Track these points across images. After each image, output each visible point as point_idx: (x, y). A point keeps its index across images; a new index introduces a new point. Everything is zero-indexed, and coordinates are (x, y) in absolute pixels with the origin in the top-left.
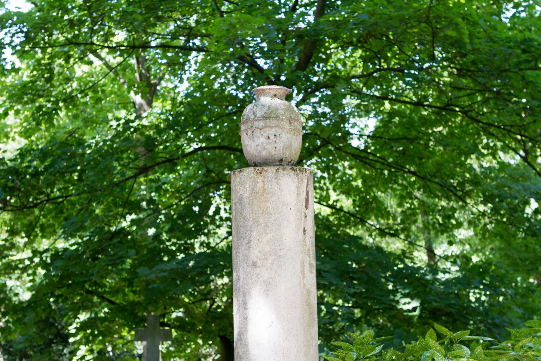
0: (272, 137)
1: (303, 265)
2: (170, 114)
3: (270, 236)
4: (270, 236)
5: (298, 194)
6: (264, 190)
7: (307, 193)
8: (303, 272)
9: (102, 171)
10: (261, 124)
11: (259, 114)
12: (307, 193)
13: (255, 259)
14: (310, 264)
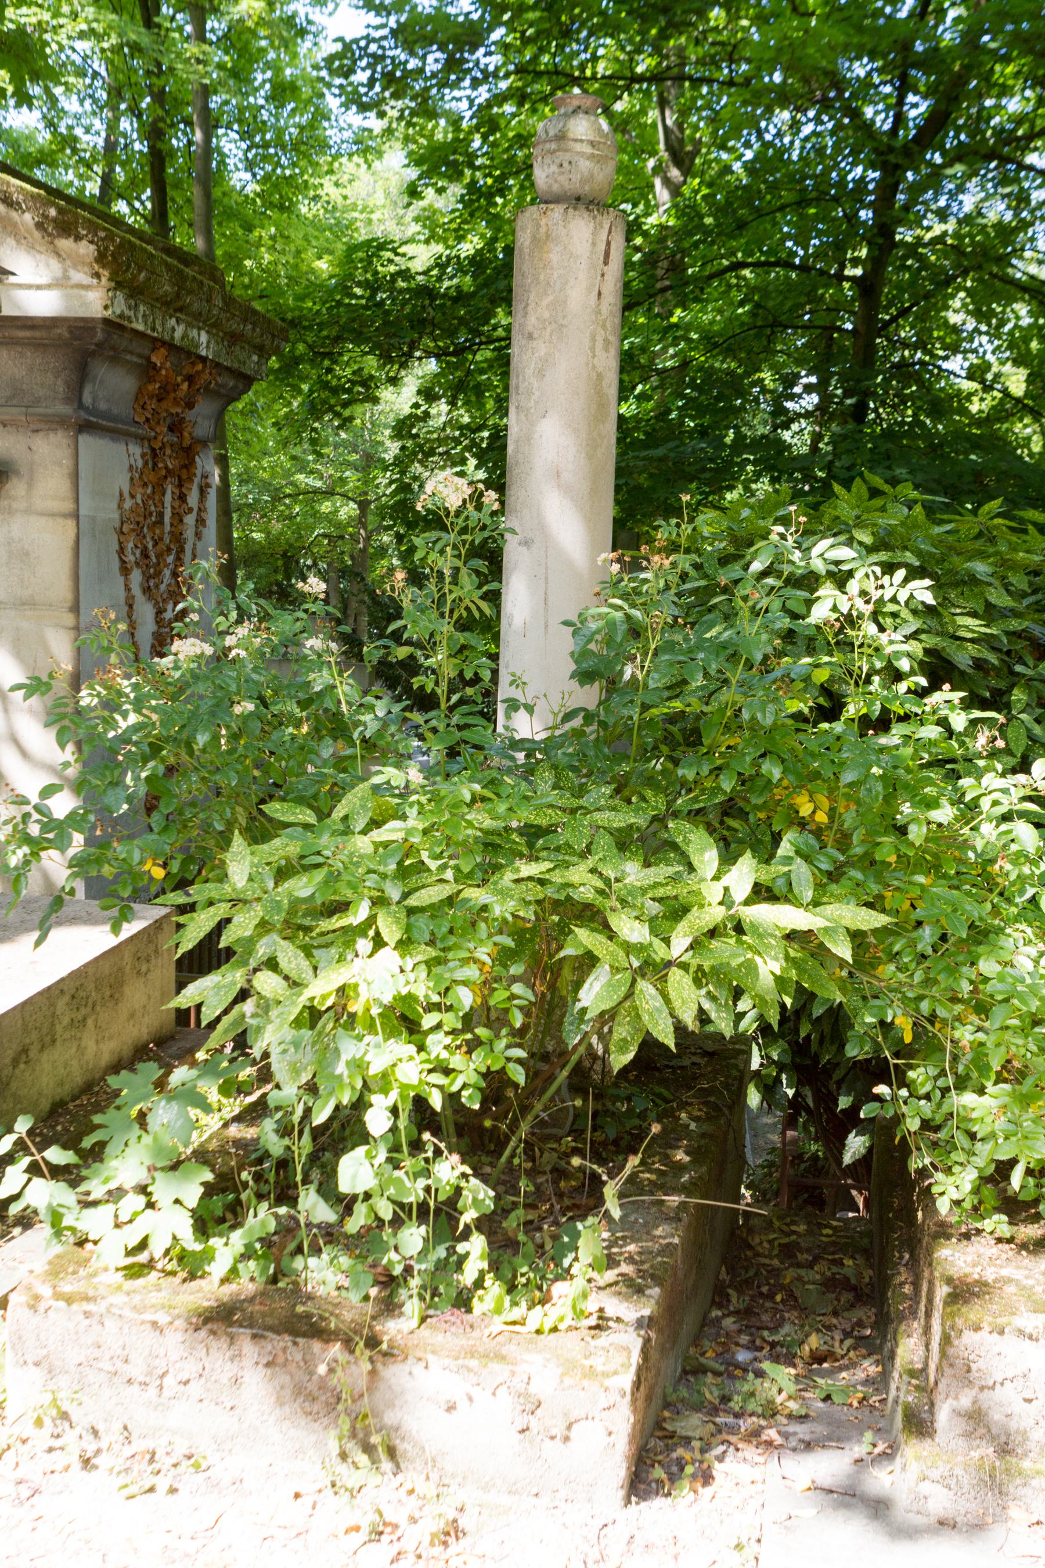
0: (566, 164)
1: (593, 339)
2: (972, 237)
3: (551, 298)
4: (551, 298)
5: (594, 244)
6: (548, 236)
7: (608, 244)
8: (593, 349)
9: (734, 657)
10: (553, 146)
11: (551, 133)
12: (608, 244)
13: (530, 328)
14: (606, 341)
